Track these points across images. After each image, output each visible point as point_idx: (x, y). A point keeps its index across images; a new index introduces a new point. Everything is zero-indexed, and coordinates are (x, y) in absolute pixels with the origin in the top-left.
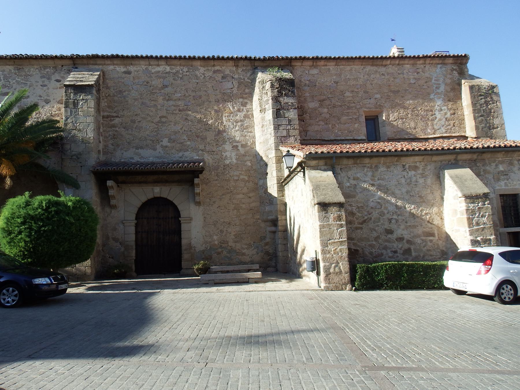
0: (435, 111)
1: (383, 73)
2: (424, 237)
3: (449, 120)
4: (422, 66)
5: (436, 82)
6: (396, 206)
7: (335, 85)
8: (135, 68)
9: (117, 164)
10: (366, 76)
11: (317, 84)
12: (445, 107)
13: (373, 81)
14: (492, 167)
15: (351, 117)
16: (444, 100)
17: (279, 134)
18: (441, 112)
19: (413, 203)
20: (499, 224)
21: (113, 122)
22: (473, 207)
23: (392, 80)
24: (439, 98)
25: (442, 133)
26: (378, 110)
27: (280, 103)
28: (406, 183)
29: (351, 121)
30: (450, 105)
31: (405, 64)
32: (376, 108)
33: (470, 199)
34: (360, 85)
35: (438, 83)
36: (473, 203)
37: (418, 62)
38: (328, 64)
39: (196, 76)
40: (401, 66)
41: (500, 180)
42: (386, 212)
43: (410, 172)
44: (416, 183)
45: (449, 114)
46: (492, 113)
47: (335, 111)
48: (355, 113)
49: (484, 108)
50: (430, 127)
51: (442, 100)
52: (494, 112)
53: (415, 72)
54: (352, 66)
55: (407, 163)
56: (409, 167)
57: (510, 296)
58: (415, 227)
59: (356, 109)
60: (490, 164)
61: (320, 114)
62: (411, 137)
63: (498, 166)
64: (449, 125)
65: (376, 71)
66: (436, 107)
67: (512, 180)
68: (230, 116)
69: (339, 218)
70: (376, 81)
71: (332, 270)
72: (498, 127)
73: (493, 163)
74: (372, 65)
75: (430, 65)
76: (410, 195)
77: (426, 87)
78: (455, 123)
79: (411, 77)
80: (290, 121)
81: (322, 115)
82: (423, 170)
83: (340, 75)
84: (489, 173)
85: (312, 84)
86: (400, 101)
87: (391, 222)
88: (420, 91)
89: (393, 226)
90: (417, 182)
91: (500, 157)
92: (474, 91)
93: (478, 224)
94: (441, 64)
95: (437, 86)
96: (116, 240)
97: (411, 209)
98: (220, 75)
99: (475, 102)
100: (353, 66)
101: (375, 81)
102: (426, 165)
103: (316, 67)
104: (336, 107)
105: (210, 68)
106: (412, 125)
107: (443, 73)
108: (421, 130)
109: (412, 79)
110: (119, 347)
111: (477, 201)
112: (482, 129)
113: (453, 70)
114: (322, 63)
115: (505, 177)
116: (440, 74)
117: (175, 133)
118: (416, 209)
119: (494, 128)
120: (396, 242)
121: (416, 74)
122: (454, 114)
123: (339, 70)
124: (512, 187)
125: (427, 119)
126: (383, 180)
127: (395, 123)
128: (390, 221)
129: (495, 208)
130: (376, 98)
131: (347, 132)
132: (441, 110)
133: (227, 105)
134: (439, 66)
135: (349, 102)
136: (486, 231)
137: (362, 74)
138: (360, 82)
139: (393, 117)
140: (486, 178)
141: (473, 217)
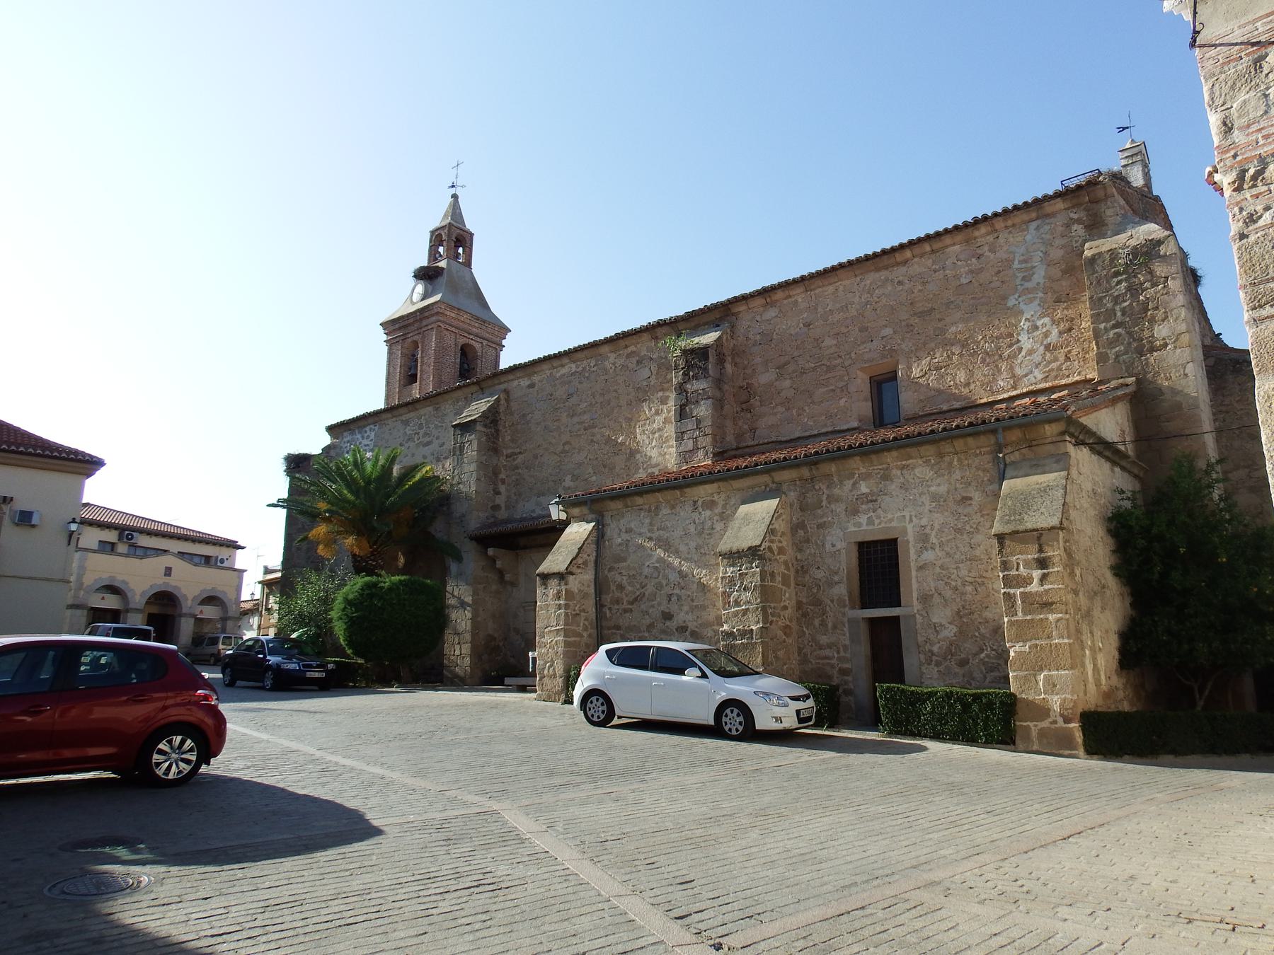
0: (1019, 334)
1: (901, 278)
3: (1055, 348)
4: (990, 238)
6: (680, 572)
7: (806, 329)
8: (539, 377)
9: (522, 520)
12: (1046, 320)
15: (833, 387)
17: (682, 449)
18: (1035, 334)
21: (516, 462)
24: (1031, 300)
25: (1036, 384)
26: (886, 360)
27: (687, 392)
29: (832, 394)
31: (947, 247)
33: (728, 558)
35: (1029, 265)
36: (733, 565)
37: (977, 233)
39: (605, 369)
41: (859, 512)
42: (664, 583)
45: (1055, 332)
50: (1005, 375)
51: (1039, 305)
52: (1157, 308)
53: (973, 257)
54: (837, 284)
56: (703, 503)
57: (727, 720)
58: (704, 608)
60: (841, 482)
62: (957, 405)
63: (857, 485)
64: (1056, 359)
65: (887, 280)
67: (885, 511)
68: (645, 424)
69: (558, 596)
71: (546, 672)
72: (1166, 345)
73: (849, 479)
74: (878, 270)
75: (1011, 229)
77: (998, 284)
78: (1069, 352)
79: (962, 270)
80: (699, 422)
82: (724, 506)
84: (838, 500)
87: (670, 600)
88: (982, 297)
89: (674, 608)
90: (713, 529)
94: (1037, 218)
95: (1025, 274)
96: (517, 631)
98: (634, 360)
103: (773, 304)
105: (621, 352)
106: (961, 376)
107: (1042, 239)
108: (982, 386)
112: (1117, 356)
114: (780, 295)
115: (870, 505)
116: (1034, 243)
117: (580, 464)
119: (1153, 349)
120: (676, 633)
122: (1070, 329)
124: (883, 525)
125: (996, 357)
126: (663, 529)
127: (921, 381)
128: (670, 597)
130: (883, 338)
131: (824, 417)
133: (643, 407)
134: (1033, 225)
137: (858, 294)
138: (853, 311)
139: (918, 370)
140: (832, 511)
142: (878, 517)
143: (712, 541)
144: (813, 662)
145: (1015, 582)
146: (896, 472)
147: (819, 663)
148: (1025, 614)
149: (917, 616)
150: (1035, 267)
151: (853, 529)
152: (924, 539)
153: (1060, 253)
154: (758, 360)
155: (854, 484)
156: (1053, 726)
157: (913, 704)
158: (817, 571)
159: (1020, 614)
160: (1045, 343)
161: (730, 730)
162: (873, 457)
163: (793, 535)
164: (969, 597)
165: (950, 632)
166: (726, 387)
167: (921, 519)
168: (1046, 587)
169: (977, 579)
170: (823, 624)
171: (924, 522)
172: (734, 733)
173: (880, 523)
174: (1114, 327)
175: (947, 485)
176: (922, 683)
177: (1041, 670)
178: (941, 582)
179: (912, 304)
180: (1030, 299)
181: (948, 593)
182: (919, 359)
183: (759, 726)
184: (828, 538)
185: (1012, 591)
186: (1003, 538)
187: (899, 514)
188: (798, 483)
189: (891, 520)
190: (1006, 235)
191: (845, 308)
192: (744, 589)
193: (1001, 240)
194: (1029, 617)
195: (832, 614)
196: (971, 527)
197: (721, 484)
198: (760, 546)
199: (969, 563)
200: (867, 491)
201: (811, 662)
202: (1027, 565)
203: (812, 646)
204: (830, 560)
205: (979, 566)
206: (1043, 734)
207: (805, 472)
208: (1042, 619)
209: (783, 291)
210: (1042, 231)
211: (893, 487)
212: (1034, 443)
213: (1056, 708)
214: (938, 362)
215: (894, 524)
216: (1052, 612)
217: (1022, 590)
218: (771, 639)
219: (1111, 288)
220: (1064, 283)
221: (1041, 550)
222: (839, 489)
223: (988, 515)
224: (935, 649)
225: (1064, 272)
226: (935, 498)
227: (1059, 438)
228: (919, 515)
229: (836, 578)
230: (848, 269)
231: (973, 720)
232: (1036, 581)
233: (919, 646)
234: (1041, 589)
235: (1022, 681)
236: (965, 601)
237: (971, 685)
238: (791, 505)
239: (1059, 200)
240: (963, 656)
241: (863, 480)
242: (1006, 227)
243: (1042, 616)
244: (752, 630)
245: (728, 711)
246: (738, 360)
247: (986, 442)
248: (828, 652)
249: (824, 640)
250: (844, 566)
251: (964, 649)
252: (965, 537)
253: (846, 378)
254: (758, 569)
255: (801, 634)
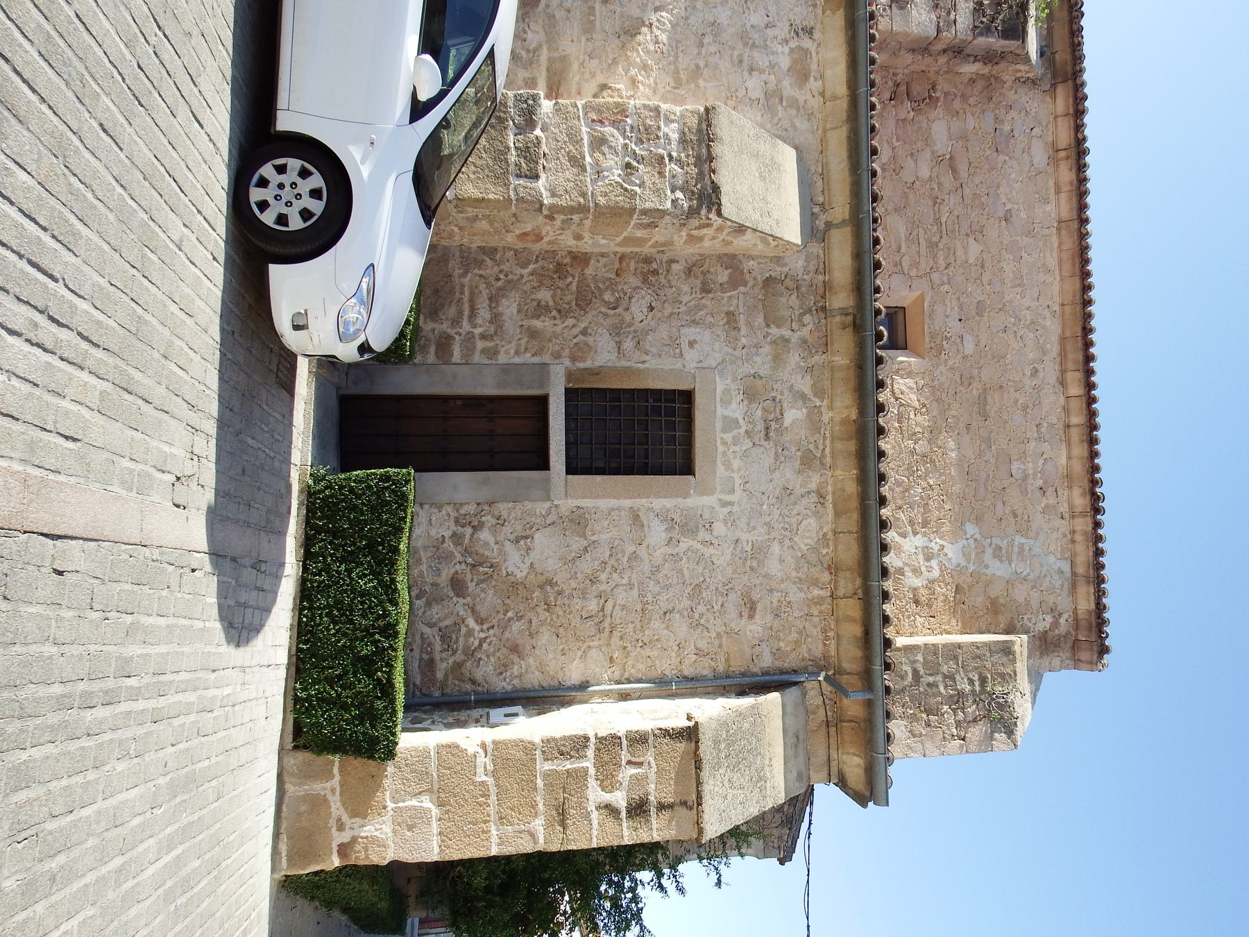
0: (925, 535)
1: (1041, 374)
2: (549, 59)
4: (1064, 508)
5: (1016, 549)
7: (1001, 214)
10: (1028, 316)
11: (1002, 158)
12: (936, 573)
13: (1015, 336)
14: (799, 377)
15: (903, 250)
16: (960, 570)
18: (921, 556)
19: (676, 43)
20: (581, 365)
22: (667, 137)
23: (1020, 402)
24: (966, 555)
26: (927, 339)
28: (748, 26)
30: (944, 591)
32: (933, 336)
33: (699, 131)
34: (1003, 293)
35: (1014, 557)
36: (683, 141)
37: (1077, 492)
38: (1063, 196)
40: (1063, 438)
43: (786, 49)
44: (745, 65)
45: (917, 582)
46: (924, 716)
47: (923, 201)
48: (915, 264)
49: (942, 689)
51: (958, 565)
52: (928, 725)
53: (1046, 482)
54: (1057, 273)
55: (819, 45)
56: (806, 52)
57: (292, 176)
58: (588, 28)
59: (928, 270)
60: (810, 370)
61: (912, 154)
63: (800, 403)
66: (938, 540)
70: (1015, 345)
73: (813, 386)
74: (1063, 340)
75: (1069, 536)
76: (703, 35)
81: (909, 157)
82: (794, 103)
83: (1029, 233)
84: (777, 360)
85: (1001, 143)
86: (953, 417)
90: (751, 70)
91: (843, 407)
92: (996, 657)
93: (599, 143)
94: (1074, 574)
97: (655, 30)
99: (961, 658)
100: (1058, 278)
101: (1015, 345)
102: (810, 116)
103: (1054, 160)
104: (935, 206)
107: (1045, 576)
109: (1022, 467)
110: (248, 643)
111: (688, 156)
113: (1055, 612)
114: (1067, 175)
115: (760, 426)
116: (1042, 565)
118: (652, 48)
121: (1040, 483)
122: (917, 602)
123: (1047, 232)
124: (721, 448)
125: (900, 502)
129: (644, 362)
132: (928, 558)
134: (1066, 567)
135: (949, 249)
136: (568, 175)
137: (1034, 304)
139: (903, 388)
140: (757, 346)
141: (628, 128)
142: (736, 441)
143: (724, 65)
144: (466, 280)
145: (606, 758)
146: (814, 481)
147: (462, 293)
148: (546, 775)
149: (548, 504)
150: (1010, 564)
151: (720, 388)
152: (685, 526)
153: (1020, 598)
154: (971, 122)
155: (803, 397)
156: (333, 822)
157: (372, 546)
158: (644, 304)
159: (548, 766)
160: (906, 568)
161: (263, 183)
162: (852, 446)
163: (720, 257)
164: (577, 603)
165: (515, 564)
166: (942, 60)
167: (726, 523)
168: (595, 815)
169: (608, 620)
170: (541, 310)
171: (719, 528)
172: (256, 194)
173: (724, 443)
174: (915, 672)
175: (779, 575)
176: (421, 505)
177: (440, 804)
178: (608, 553)
179: (1001, 387)
180: (970, 553)
181: (586, 566)
182: (920, 390)
183: (278, 274)
184: (707, 334)
185: (590, 753)
186: (690, 739)
187: (738, 481)
188: (821, 278)
189: (728, 466)
190: (1062, 530)
191: (1019, 283)
192: (628, 166)
193: (1058, 523)
194: (540, 783)
195: (559, 329)
196: (701, 615)
197: (843, 104)
198: (719, 214)
199: (639, 607)
200: (788, 421)
201: (466, 272)
202: (637, 781)
203: (498, 279)
204: (665, 335)
205: (631, 626)
206: (317, 803)
207: (842, 300)
208: (534, 806)
209: (1071, 183)
210: (1056, 577)
211: (788, 474)
212: (833, 730)
213: (368, 830)
214: (909, 419)
215: (721, 470)
216: (548, 825)
217: (592, 771)
218: (515, 215)
219: (966, 672)
220: (980, 599)
221: (662, 807)
222: (798, 364)
223: (720, 646)
224: (485, 535)
225: (994, 602)
226: (759, 552)
227: (834, 771)
228: (731, 521)
229: (628, 344)
230: (1078, 297)
231: (340, 677)
232: (607, 797)
233: (490, 504)
234: (591, 807)
235: (419, 767)
236: (571, 596)
237: (418, 597)
238: (778, 260)
239: (1093, 606)
240: (471, 586)
241: (808, 416)
242: (1074, 532)
243: (541, 806)
244: (537, 177)
245: (317, 181)
246: (980, 84)
247: (850, 657)
248: (484, 313)
249: (509, 308)
250: (652, 363)
251: (483, 590)
252: (686, 603)
253: (913, 273)
254: (668, 205)
255: (522, 257)
